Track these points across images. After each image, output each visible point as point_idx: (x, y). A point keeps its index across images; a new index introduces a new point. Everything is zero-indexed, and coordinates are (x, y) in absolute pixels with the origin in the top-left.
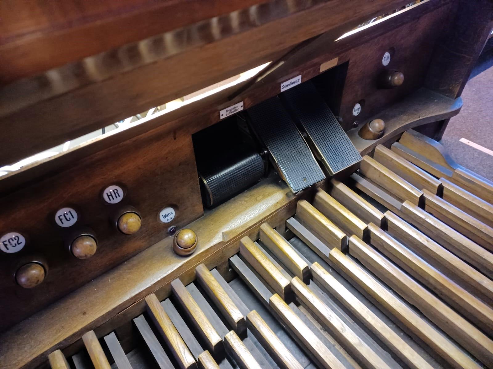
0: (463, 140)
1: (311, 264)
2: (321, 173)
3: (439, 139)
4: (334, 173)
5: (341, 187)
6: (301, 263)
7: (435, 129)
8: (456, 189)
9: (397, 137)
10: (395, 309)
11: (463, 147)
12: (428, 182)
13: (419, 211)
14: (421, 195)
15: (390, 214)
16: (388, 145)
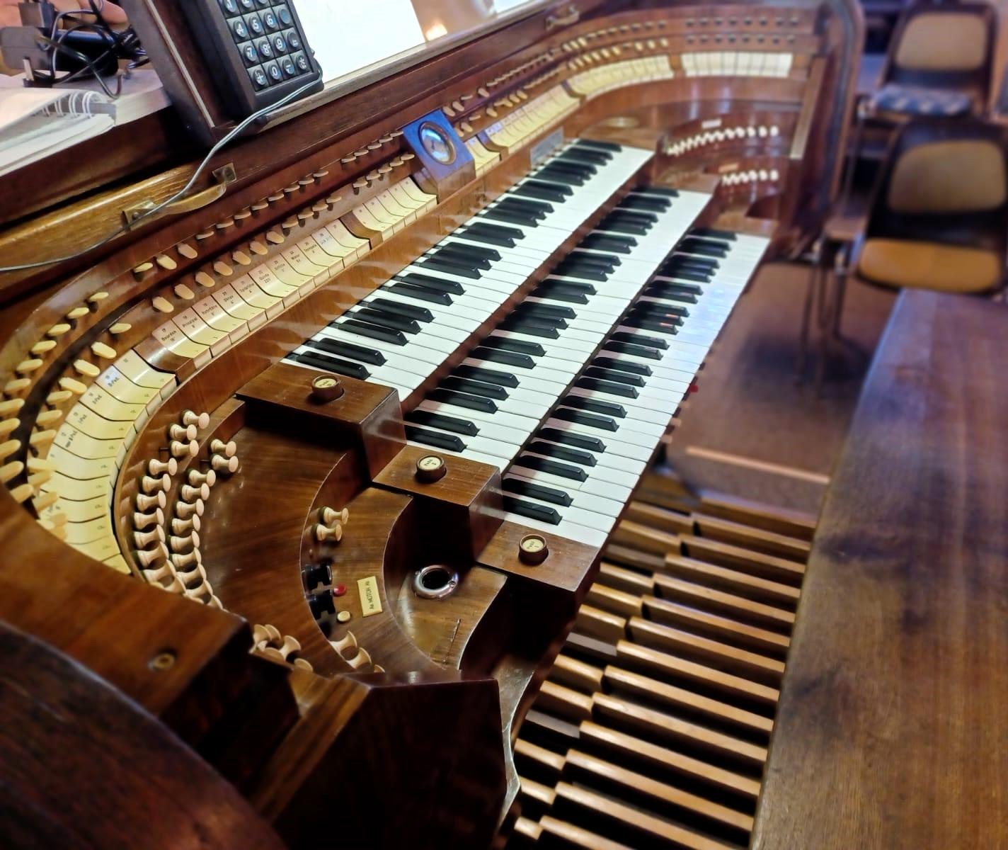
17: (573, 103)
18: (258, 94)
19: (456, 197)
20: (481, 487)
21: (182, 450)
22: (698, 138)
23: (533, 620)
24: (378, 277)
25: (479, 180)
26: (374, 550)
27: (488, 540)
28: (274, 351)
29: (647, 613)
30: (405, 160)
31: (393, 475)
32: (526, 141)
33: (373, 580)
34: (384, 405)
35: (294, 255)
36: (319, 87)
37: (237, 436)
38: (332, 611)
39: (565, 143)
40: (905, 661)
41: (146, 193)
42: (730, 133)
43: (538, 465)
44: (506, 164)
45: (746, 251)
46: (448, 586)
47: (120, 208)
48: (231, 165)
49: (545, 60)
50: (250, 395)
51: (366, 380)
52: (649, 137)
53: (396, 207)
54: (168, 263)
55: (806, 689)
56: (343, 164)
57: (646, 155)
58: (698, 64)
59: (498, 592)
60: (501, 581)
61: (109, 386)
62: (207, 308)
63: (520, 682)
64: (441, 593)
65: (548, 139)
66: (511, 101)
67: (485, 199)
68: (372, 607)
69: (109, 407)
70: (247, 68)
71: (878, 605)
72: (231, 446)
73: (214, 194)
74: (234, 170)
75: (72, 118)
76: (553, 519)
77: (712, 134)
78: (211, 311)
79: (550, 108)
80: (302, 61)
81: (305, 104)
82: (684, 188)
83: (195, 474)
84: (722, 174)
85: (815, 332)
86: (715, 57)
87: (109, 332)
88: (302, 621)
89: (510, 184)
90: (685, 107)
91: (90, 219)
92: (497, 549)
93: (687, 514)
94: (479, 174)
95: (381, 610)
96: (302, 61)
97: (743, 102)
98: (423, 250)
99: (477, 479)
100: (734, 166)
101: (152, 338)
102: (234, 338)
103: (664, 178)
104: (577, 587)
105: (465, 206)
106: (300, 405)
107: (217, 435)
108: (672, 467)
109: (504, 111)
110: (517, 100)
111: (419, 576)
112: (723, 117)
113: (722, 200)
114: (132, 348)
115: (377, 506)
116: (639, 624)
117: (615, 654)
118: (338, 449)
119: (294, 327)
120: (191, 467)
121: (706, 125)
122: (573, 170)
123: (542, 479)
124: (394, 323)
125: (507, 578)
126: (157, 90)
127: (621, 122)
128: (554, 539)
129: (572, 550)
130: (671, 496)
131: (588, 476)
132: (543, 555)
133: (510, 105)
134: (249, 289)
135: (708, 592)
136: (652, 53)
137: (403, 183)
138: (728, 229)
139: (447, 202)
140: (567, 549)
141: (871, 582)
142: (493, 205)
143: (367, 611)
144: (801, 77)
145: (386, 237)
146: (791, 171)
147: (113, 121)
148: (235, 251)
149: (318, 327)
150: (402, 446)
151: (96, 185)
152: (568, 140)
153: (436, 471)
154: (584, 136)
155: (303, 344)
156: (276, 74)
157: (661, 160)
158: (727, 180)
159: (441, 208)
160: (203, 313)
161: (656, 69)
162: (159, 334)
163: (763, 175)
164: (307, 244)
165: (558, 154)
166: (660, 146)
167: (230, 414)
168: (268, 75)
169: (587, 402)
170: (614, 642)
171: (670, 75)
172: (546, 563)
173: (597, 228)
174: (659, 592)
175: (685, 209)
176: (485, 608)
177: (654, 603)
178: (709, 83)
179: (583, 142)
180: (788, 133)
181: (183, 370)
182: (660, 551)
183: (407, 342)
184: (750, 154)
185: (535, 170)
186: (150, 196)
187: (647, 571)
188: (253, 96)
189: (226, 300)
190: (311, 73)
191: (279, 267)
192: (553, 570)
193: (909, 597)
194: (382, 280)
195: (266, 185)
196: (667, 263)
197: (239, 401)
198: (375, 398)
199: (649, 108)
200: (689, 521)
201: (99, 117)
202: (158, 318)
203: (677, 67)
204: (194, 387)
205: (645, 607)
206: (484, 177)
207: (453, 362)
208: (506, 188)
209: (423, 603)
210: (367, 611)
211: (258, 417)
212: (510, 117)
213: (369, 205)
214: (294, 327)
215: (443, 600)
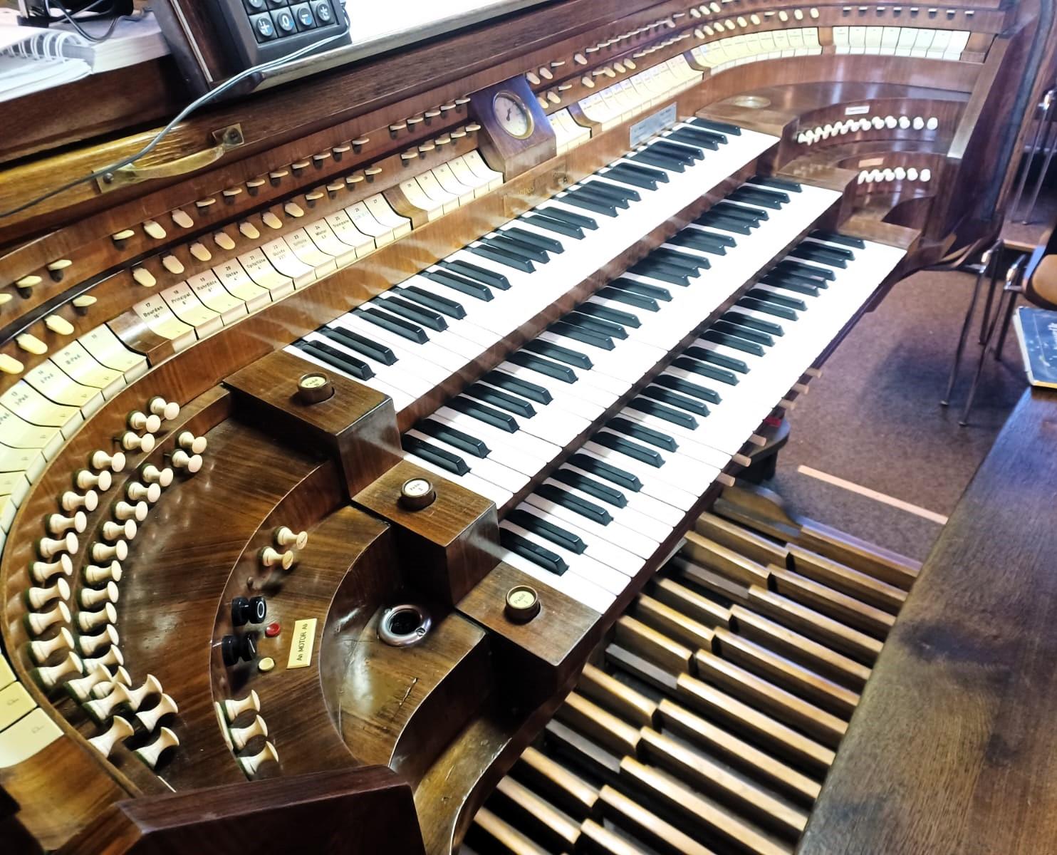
0: (803, 469)
1: (34, 289)
5: (667, 585)
6: (646, 706)
8: (809, 556)
10: (579, 697)
11: (806, 481)
12: (772, 554)
13: (788, 575)
14: (768, 574)
15: (738, 610)
17: (695, 77)
18: (261, 46)
19: (528, 176)
20: (467, 524)
21: (135, 443)
22: (839, 125)
23: (509, 692)
24: (418, 259)
25: (561, 158)
26: (328, 585)
27: (476, 583)
28: (279, 334)
29: (718, 648)
30: (476, 127)
31: (376, 495)
32: (626, 118)
33: (312, 623)
34: (371, 416)
35: (319, 231)
36: (346, 40)
37: (218, 430)
38: (251, 657)
39: (678, 121)
40: (981, 804)
41: (123, 152)
42: (878, 123)
43: (558, 497)
44: (597, 140)
45: (875, 259)
46: (415, 634)
47: (89, 168)
48: (238, 126)
49: (665, 26)
50: (237, 386)
52: (778, 122)
53: (452, 183)
54: (157, 231)
55: (847, 812)
56: (392, 131)
57: (773, 140)
58: (854, 40)
59: (469, 651)
60: (476, 637)
61: (66, 364)
62: (204, 283)
63: (486, 756)
64: (411, 639)
65: (656, 115)
66: (615, 71)
67: (566, 179)
68: (300, 658)
69: (57, 386)
70: (248, 15)
71: (960, 723)
72: (200, 443)
73: (204, 158)
74: (240, 131)
75: (47, 61)
76: (558, 567)
77: (857, 121)
78: (208, 288)
79: (670, 78)
80: (324, 11)
81: (316, 62)
82: (809, 182)
83: (150, 471)
84: (861, 170)
85: (972, 348)
86: (874, 33)
87: (73, 305)
88: (196, 674)
89: (600, 164)
90: (826, 88)
91: (46, 177)
92: (483, 597)
93: (782, 543)
94: (560, 151)
95: (308, 664)
96: (324, 11)
97: (891, 84)
98: (480, 233)
99: (466, 514)
100: (878, 161)
101: (133, 313)
102: (227, 320)
103: (792, 169)
105: (539, 186)
106: (284, 407)
107: (188, 427)
108: (778, 491)
109: (605, 83)
110: (622, 70)
111: (389, 614)
112: (871, 102)
113: (852, 200)
114: (105, 323)
115: (353, 530)
116: (704, 657)
117: (674, 687)
118: (312, 459)
119: (308, 307)
120: (147, 462)
121: (849, 111)
122: (676, 155)
123: (558, 516)
124: (420, 316)
125: (484, 634)
126: (153, 36)
127: (750, 102)
128: (548, 596)
129: (569, 611)
130: (768, 520)
131: (612, 519)
132: (533, 611)
133: (612, 74)
134: (258, 265)
135: (791, 636)
136: (799, 25)
137: (467, 157)
138: (855, 234)
139: (515, 182)
140: (563, 608)
141: (952, 687)
142: (574, 188)
143: (293, 662)
144: (975, 60)
145: (433, 217)
146: (947, 172)
147: (89, 68)
148: (243, 222)
149: (338, 312)
150: (397, 460)
151: (58, 144)
152: (682, 118)
153: (421, 498)
154: (702, 115)
155: (316, 331)
156: (287, 25)
157: (789, 146)
158: (864, 176)
159: (507, 187)
160: (198, 288)
161: (803, 43)
162: (141, 308)
163: (912, 174)
164: (337, 218)
165: (667, 133)
166: (789, 132)
167: (210, 404)
168: (277, 25)
169: (635, 427)
170: (675, 673)
171: (817, 51)
172: (535, 623)
173: (695, 222)
174: (735, 626)
175: (808, 204)
176: (448, 669)
177: (727, 638)
178: (856, 61)
179: (699, 122)
180: (948, 129)
181: (157, 353)
182: (746, 580)
183: (428, 340)
184: (897, 148)
185: (635, 150)
186: (143, 153)
187: (725, 601)
188: (252, 47)
189: (228, 276)
190: (335, 26)
191: (299, 242)
192: (539, 634)
193: (999, 717)
194: (424, 263)
195: (291, 151)
197: (225, 390)
199: (785, 87)
200: (782, 552)
201: (75, 62)
202: (140, 293)
203: (826, 43)
204: (167, 372)
205: (716, 640)
206: (567, 156)
207: (485, 365)
208: (594, 168)
209: (383, 649)
210: (293, 662)
211: (242, 410)
212: (612, 88)
213: (420, 179)
214: (308, 307)
215: (405, 648)
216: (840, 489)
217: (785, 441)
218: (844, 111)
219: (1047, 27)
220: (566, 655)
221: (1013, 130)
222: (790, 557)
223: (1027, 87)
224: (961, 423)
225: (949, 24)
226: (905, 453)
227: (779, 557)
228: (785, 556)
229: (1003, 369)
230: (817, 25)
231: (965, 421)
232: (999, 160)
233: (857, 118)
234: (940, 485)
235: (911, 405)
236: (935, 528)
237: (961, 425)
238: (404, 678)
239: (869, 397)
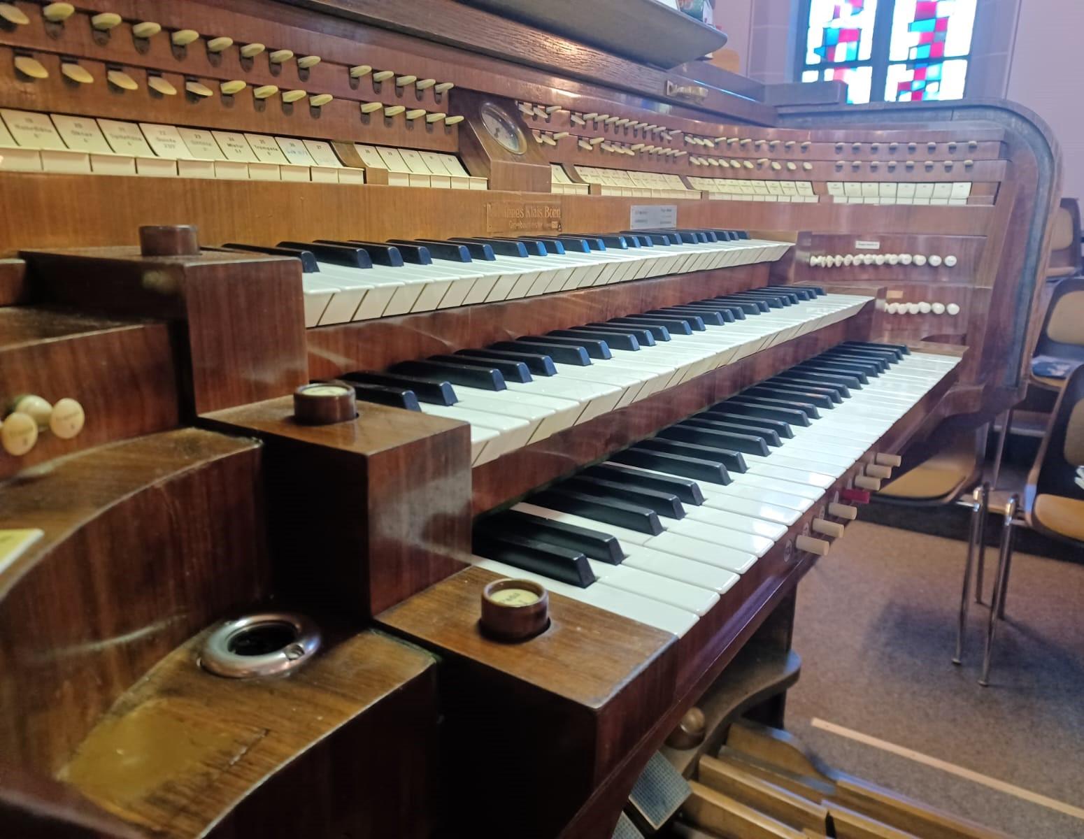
0: (817, 723)
2: (627, 821)
3: (780, 726)
4: (656, 828)
7: (768, 712)
9: (723, 736)
12: (806, 814)
16: (713, 752)
35: (232, 143)
46: (282, 655)
51: (659, 517)
58: (844, 193)
59: (398, 686)
104: (605, 701)
121: (859, 245)
163: (938, 308)
196: (401, 689)
198: (149, 421)
215: (256, 683)
216: (865, 746)
217: (795, 677)
218: (854, 244)
219: (1047, 185)
220: (613, 694)
221: (1027, 291)
222: (830, 821)
223: (1035, 246)
224: (982, 682)
225: (947, 176)
226: (927, 715)
227: (815, 819)
228: (823, 816)
229: (1010, 628)
230: (812, 179)
231: (986, 681)
232: (1016, 324)
233: (865, 252)
234: (979, 753)
235: (919, 662)
236: (996, 797)
237: (982, 685)
238: (237, 730)
239: (871, 653)
